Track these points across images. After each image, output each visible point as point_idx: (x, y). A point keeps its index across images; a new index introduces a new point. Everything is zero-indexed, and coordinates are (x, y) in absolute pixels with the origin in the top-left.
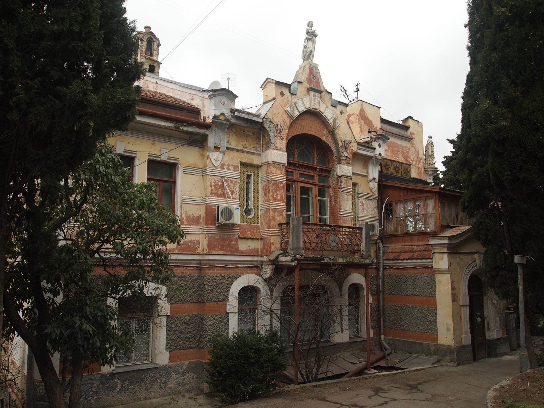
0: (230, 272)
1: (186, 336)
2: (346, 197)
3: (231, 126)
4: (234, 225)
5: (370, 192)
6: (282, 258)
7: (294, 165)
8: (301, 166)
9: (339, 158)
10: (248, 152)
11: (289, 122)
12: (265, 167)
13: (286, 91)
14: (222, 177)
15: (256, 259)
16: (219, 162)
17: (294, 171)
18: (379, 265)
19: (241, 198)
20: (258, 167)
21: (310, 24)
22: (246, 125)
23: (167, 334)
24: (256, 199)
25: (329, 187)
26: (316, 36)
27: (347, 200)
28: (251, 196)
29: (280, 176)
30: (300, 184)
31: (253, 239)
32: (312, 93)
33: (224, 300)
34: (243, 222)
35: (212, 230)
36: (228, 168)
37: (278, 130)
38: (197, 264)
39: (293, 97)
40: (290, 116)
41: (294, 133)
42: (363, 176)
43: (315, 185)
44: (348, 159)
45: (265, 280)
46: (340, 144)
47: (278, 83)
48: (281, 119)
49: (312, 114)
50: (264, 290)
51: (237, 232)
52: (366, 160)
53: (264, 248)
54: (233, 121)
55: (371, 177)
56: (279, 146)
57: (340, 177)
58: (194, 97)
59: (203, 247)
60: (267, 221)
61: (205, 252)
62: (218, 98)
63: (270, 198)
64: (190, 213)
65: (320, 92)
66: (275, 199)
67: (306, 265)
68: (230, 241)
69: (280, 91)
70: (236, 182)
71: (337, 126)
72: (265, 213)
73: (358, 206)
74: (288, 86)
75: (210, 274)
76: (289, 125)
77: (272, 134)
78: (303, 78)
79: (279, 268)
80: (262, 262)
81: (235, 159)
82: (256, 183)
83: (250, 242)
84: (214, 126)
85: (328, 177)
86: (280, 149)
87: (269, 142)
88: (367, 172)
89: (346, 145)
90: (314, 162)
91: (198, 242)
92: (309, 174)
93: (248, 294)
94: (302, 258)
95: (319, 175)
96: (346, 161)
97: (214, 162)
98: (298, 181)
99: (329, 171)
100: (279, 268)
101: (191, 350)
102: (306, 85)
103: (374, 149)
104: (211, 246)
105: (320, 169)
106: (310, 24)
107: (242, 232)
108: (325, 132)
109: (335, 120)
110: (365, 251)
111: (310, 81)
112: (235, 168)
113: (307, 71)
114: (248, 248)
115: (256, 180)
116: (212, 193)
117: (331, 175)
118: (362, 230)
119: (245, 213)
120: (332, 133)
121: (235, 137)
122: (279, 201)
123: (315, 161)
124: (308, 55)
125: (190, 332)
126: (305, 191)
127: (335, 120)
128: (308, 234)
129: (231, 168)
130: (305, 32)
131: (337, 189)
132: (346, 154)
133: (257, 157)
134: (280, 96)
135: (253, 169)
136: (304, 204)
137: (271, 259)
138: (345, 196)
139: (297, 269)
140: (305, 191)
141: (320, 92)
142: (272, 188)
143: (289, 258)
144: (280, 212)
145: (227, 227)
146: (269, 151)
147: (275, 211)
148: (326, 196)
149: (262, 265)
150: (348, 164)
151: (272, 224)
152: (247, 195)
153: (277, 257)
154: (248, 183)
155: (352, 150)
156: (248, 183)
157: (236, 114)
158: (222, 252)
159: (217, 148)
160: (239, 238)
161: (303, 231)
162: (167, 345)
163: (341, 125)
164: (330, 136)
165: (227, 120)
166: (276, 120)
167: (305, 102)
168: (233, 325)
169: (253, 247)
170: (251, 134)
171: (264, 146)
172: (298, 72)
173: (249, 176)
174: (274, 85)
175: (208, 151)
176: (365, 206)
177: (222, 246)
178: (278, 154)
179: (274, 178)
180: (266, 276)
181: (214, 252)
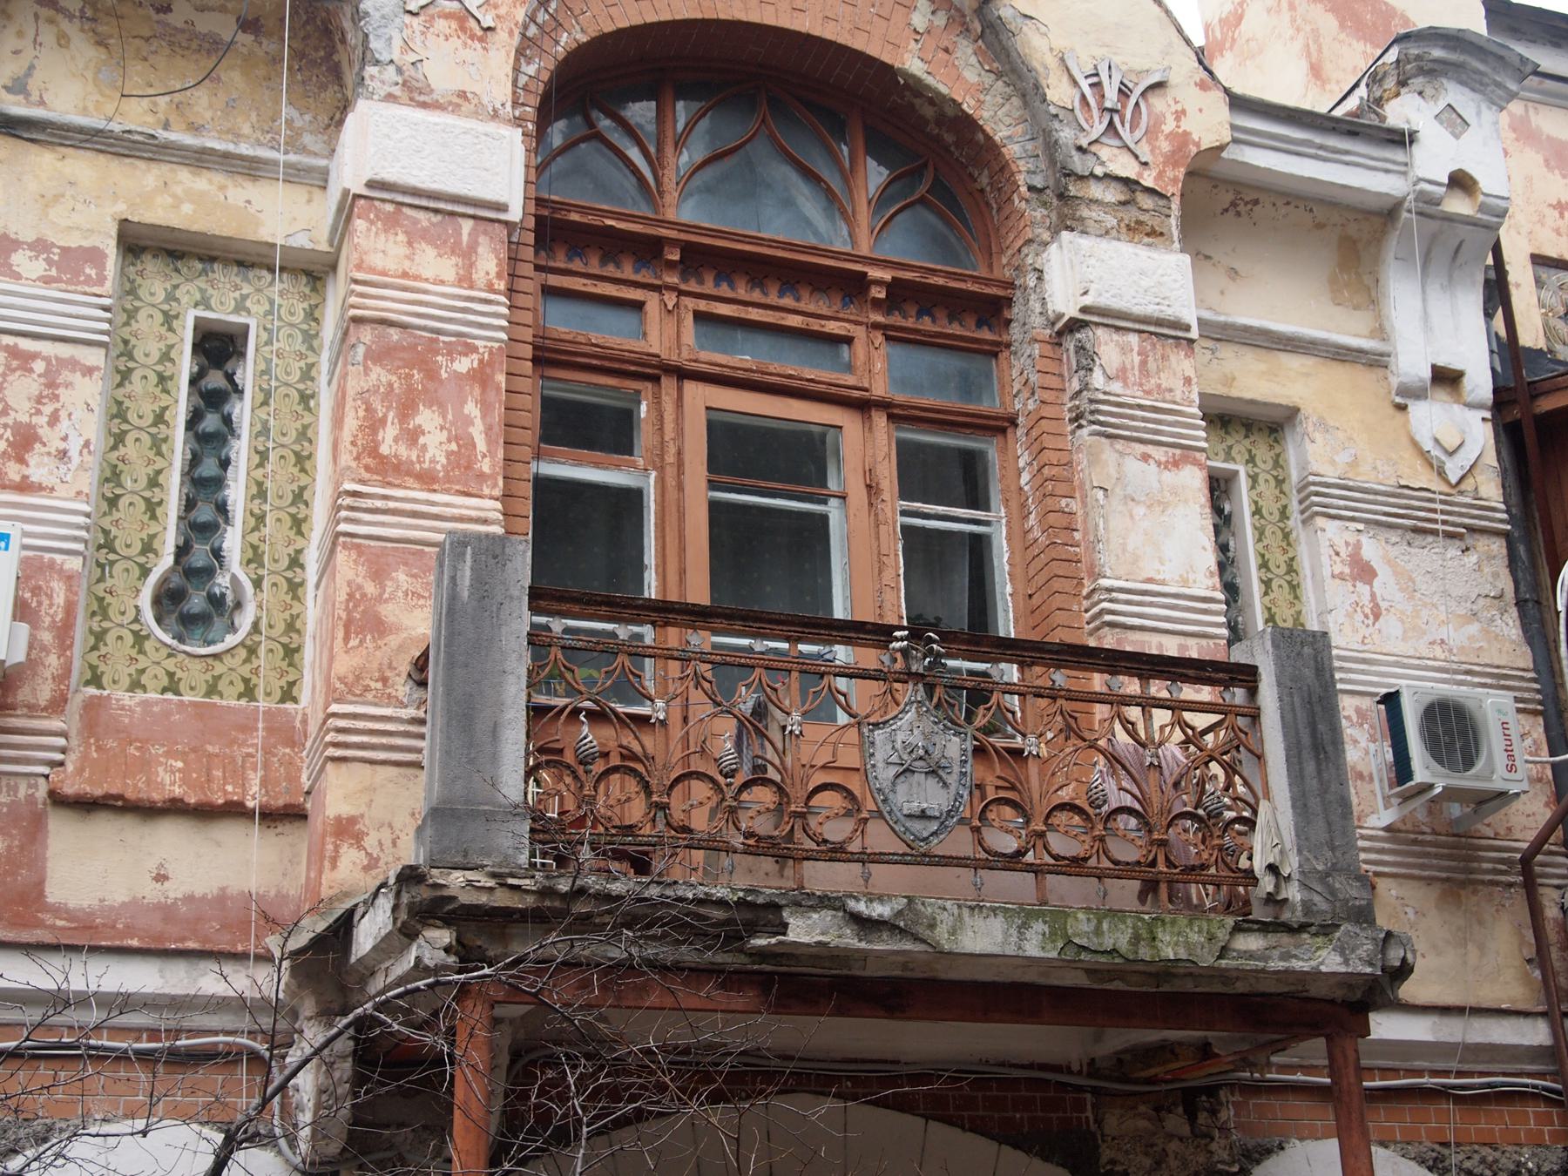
5: (1423, 478)
9: (1062, 196)
10: (200, 159)
15: (209, 981)
17: (652, 301)
25: (1001, 426)
29: (460, 293)
30: (699, 396)
31: (205, 813)
34: (136, 685)
42: (1342, 355)
43: (863, 406)
44: (1147, 202)
46: (1059, 93)
52: (1354, 238)
55: (1413, 363)
57: (1074, 326)
70: (73, 364)
73: (1319, 587)
81: (792, 936)
85: (993, 351)
88: (1381, 332)
89: (1126, 101)
92: (795, 321)
94: (502, 899)
96: (1131, 214)
98: (682, 374)
99: (993, 308)
103: (1401, 139)
105: (894, 287)
110: (1291, 866)
114: (151, 892)
117: (1015, 332)
118: (1253, 692)
121: (84, 51)
122: (427, 479)
132: (1125, 167)
133: (298, 194)
138: (1133, 466)
160: (58, 800)
176: (1385, 584)
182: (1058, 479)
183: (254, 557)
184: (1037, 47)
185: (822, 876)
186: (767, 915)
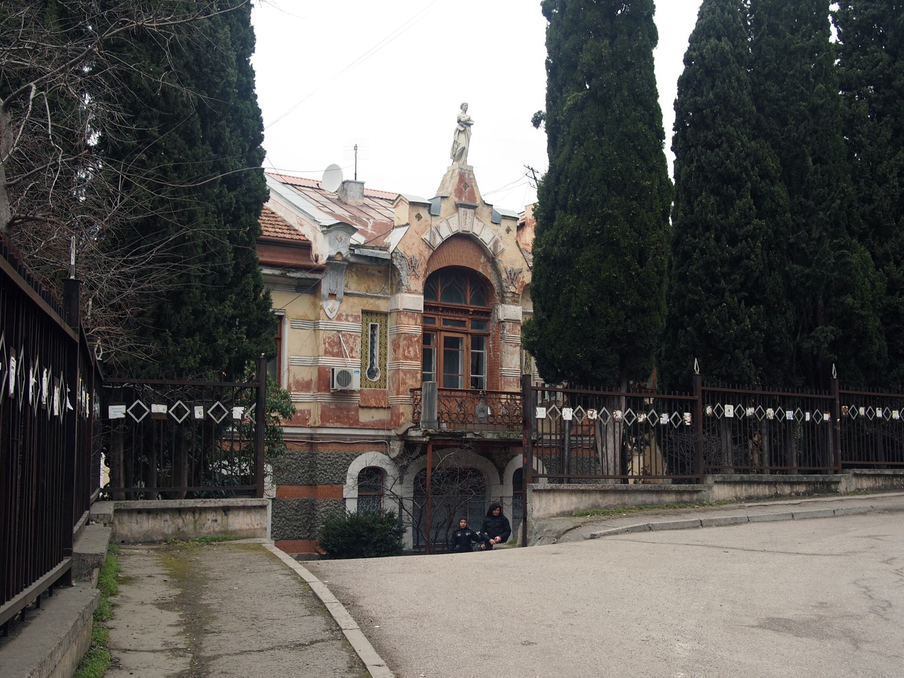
0: (347, 449)
1: (294, 524)
2: (510, 349)
3: (351, 265)
4: (353, 391)
6: (413, 433)
7: (436, 308)
8: (446, 309)
10: (372, 297)
11: (427, 253)
12: (394, 315)
13: (424, 213)
14: (339, 331)
15: (381, 433)
16: (335, 313)
18: (564, 444)
19: (363, 356)
20: (386, 314)
21: (464, 107)
22: (367, 263)
23: (273, 520)
24: (383, 356)
25: (488, 335)
26: (469, 125)
27: (512, 354)
28: (377, 352)
29: (414, 328)
30: (444, 334)
32: (462, 210)
33: (339, 483)
35: (325, 398)
36: (347, 320)
37: (412, 266)
38: (308, 438)
39: (434, 218)
40: (429, 246)
41: (436, 266)
43: (467, 334)
45: (393, 459)
46: (504, 276)
47: (413, 204)
48: (417, 251)
49: (464, 238)
50: (391, 470)
51: (357, 399)
53: (392, 419)
54: (352, 260)
56: (413, 288)
58: (303, 222)
59: (315, 418)
60: (396, 386)
61: (317, 425)
62: (333, 234)
63: (400, 356)
64: (299, 377)
65: (474, 207)
66: (406, 358)
67: (440, 442)
68: (348, 411)
69: (415, 213)
71: (499, 250)
72: (394, 374)
74: (427, 206)
75: (322, 451)
76: (427, 258)
77: (403, 273)
78: (450, 189)
79: (409, 446)
80: (390, 437)
81: (356, 306)
82: (384, 335)
83: (373, 412)
84: (328, 268)
85: (488, 321)
86: (415, 292)
87: (400, 283)
90: (466, 303)
91: (309, 411)
93: (371, 475)
95: (472, 319)
97: (328, 313)
99: (488, 314)
100: (409, 446)
101: (300, 541)
102: (454, 199)
104: (324, 417)
105: (473, 312)
106: (464, 107)
107: (364, 400)
108: (482, 261)
109: (496, 242)
111: (459, 192)
112: (356, 318)
113: (456, 179)
114: (372, 419)
115: (383, 332)
116: (327, 353)
119: (369, 374)
120: (492, 260)
121: (355, 278)
122: (411, 359)
123: (468, 303)
124: (459, 154)
125: (299, 520)
126: (452, 344)
127: (496, 242)
128: (446, 403)
129: (351, 319)
130: (456, 120)
131: (499, 338)
132: (513, 289)
134: (416, 220)
135: (379, 318)
136: (451, 359)
137: (400, 433)
139: (430, 447)
140: (452, 344)
141: (474, 207)
142: (403, 343)
143: (419, 433)
144: (413, 373)
145: (346, 394)
146: (399, 295)
147: (405, 372)
148: (485, 347)
149: (389, 441)
150: (515, 302)
151: (401, 389)
152: (372, 351)
153: (407, 431)
154: (373, 336)
155: (523, 282)
156: (373, 336)
157: (357, 252)
158: (338, 425)
159: (332, 295)
161: (439, 400)
162: (272, 533)
163: (507, 249)
164: (489, 266)
165: (345, 260)
166: (409, 253)
167: (449, 224)
168: (352, 507)
169: (378, 419)
170: (376, 272)
171: (394, 287)
172: (445, 176)
173: (373, 327)
174: (408, 206)
175: (321, 300)
177: (339, 417)
178: (411, 299)
179: (406, 330)
180: (393, 455)
181: (328, 425)
182: (497, 349)
183: (380, 365)
184: (501, 266)
185: (470, 426)
186: (464, 434)
